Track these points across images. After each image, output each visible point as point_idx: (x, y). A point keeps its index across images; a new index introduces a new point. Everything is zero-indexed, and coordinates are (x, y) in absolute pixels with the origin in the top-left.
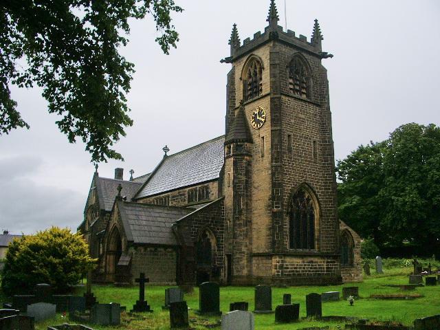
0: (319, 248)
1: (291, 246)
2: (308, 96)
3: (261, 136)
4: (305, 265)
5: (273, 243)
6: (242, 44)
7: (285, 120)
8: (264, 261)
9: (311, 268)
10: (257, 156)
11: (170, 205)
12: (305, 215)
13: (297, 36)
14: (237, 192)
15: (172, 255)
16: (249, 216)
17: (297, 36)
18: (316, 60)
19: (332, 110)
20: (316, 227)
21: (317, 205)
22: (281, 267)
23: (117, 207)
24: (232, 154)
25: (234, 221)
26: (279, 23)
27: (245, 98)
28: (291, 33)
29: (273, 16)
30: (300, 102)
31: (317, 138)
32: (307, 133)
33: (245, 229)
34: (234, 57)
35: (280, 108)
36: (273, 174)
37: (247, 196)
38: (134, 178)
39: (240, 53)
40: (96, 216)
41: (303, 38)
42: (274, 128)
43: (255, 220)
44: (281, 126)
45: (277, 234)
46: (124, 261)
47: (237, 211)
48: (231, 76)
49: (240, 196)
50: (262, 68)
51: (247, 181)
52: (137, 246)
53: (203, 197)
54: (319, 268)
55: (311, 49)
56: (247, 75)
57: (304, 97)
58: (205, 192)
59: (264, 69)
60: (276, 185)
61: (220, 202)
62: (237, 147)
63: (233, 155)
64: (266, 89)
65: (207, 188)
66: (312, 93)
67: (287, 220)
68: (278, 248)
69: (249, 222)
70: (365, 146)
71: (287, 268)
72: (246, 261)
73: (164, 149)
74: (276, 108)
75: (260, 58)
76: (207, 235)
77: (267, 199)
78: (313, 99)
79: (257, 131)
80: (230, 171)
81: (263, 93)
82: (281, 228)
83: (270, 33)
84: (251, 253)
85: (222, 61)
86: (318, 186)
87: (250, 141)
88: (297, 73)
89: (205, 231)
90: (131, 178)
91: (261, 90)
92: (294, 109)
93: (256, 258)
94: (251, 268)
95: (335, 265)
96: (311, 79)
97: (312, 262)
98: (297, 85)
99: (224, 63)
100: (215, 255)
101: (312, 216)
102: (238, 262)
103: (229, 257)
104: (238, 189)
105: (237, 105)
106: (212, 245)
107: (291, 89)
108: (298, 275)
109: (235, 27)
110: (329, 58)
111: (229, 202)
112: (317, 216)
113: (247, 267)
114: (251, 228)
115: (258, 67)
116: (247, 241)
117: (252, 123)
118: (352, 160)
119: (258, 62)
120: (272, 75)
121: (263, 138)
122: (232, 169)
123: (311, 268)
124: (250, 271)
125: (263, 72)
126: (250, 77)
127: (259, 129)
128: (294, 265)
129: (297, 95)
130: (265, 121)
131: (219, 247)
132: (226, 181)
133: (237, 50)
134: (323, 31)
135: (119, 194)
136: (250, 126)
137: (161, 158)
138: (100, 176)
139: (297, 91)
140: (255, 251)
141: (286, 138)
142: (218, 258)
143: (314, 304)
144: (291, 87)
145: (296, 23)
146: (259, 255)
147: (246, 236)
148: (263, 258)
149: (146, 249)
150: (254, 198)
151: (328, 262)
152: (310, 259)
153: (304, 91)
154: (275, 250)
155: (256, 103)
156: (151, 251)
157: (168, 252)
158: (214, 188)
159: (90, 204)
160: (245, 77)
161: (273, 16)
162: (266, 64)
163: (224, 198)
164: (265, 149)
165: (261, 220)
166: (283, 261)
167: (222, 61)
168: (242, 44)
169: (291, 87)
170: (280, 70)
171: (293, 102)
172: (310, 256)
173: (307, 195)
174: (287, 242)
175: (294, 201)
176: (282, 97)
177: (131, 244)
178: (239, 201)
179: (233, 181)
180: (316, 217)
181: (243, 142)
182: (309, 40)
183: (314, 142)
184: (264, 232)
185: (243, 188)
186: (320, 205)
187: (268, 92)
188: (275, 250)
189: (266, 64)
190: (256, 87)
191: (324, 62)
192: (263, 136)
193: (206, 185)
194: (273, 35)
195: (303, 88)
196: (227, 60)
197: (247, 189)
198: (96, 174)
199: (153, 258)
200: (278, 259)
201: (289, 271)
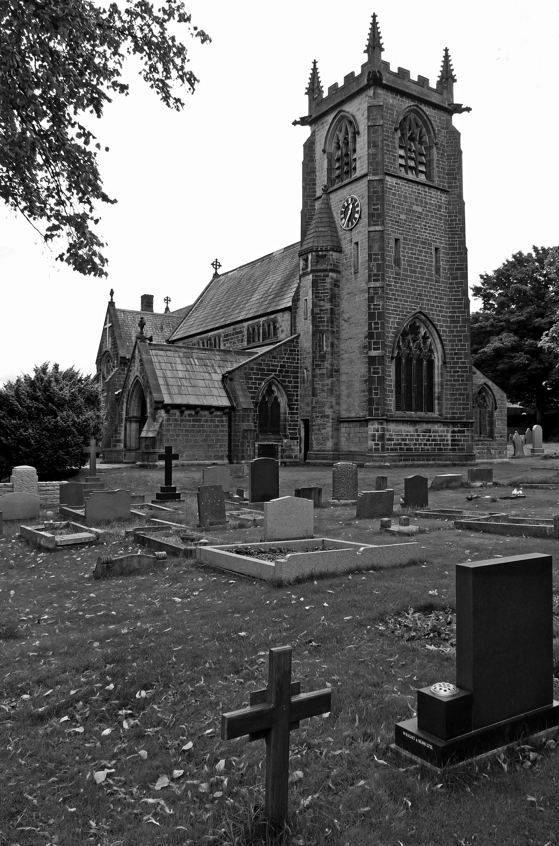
0: (440, 410)
1: (398, 408)
2: (428, 175)
3: (354, 241)
4: (418, 435)
5: (370, 401)
6: (325, 94)
7: (391, 213)
8: (357, 429)
9: (428, 440)
10: (348, 273)
11: (222, 347)
12: (420, 362)
13: (414, 77)
14: (316, 326)
15: (222, 421)
16: (335, 362)
17: (414, 77)
18: (444, 116)
19: (465, 198)
20: (437, 379)
21: (439, 346)
22: (382, 437)
23: (139, 352)
24: (309, 269)
25: (313, 370)
26: (384, 57)
27: (331, 181)
28: (403, 73)
29: (374, 45)
30: (415, 187)
31: (442, 244)
32: (425, 235)
33: (329, 381)
34: (314, 116)
35: (383, 196)
36: (371, 300)
37: (333, 332)
38: (172, 310)
39: (324, 108)
40: (114, 367)
41: (423, 81)
42: (372, 228)
43: (344, 368)
44: (383, 224)
45: (376, 389)
46: (148, 432)
47: (318, 357)
48: (309, 147)
49: (322, 332)
50: (356, 133)
51: (332, 310)
52: (168, 408)
53: (269, 335)
54: (441, 440)
55: (435, 99)
56: (334, 145)
57: (422, 178)
58: (272, 327)
59: (358, 133)
60: (375, 316)
61: (294, 343)
62: (319, 258)
63: (312, 271)
64: (362, 167)
65: (275, 322)
66: (435, 171)
67: (392, 369)
68: (377, 409)
69: (335, 372)
70: (525, 254)
71: (392, 440)
72: (330, 429)
73: (213, 264)
74: (377, 196)
75: (354, 117)
76: (273, 392)
77: (362, 336)
78: (436, 183)
79: (348, 234)
80: (307, 295)
81: (358, 174)
82: (382, 380)
83: (369, 73)
84: (339, 418)
85: (295, 123)
86: (441, 319)
87: (339, 250)
88: (412, 139)
89: (270, 386)
90: (167, 309)
91: (355, 168)
92: (405, 197)
93: (346, 425)
94: (338, 438)
95: (465, 436)
96: (434, 149)
97: (429, 431)
98: (412, 159)
99: (298, 126)
100: (285, 420)
101: (431, 363)
102: (319, 430)
103: (306, 422)
104: (320, 322)
105: (319, 192)
106: (282, 405)
107: (401, 165)
108: (408, 449)
109: (315, 66)
110: (465, 113)
111: (306, 343)
112: (438, 363)
113: (332, 438)
114: (338, 381)
115: (350, 130)
116: (334, 400)
117: (342, 223)
118: (502, 278)
119: (351, 123)
120: (372, 144)
121: (357, 243)
122: (310, 292)
123: (428, 440)
124: (337, 444)
125: (358, 139)
126: (338, 147)
127: (351, 230)
128: (402, 435)
129: (411, 176)
130: (360, 217)
131: (290, 409)
132: (301, 312)
133: (318, 105)
134: (457, 70)
135: (142, 333)
136: (338, 226)
137: (211, 278)
138: (117, 306)
139: (412, 168)
140: (344, 414)
141: (392, 244)
142: (290, 425)
143: (416, 493)
144: (402, 162)
145: (412, 57)
146: (349, 421)
147: (331, 391)
148: (355, 424)
149: (182, 412)
150: (344, 335)
151: (453, 432)
152: (426, 426)
153: (422, 168)
154: (374, 412)
155: (347, 189)
156: (190, 415)
157: (216, 416)
158: (284, 320)
159: (104, 350)
160: (332, 148)
161: (374, 45)
162: (363, 125)
163: (299, 336)
164: (360, 260)
165: (353, 367)
166: (383, 429)
167: (295, 123)
168: (325, 94)
169: (402, 162)
170: (386, 133)
171: (404, 187)
172: (428, 422)
173: (423, 331)
174: (391, 400)
175: (403, 341)
176: (388, 178)
177: (160, 405)
178: (321, 340)
179: (313, 310)
180: (436, 363)
181: (327, 250)
182: (433, 84)
183: (437, 249)
184: (359, 386)
185: (326, 322)
186: (443, 346)
187: (365, 171)
188: (374, 412)
189: (363, 125)
190: (347, 164)
191: (457, 120)
192: (356, 241)
193: (273, 316)
194: (376, 76)
195: (421, 163)
196: (303, 121)
197: (332, 322)
198: (111, 304)
199: (194, 426)
200: (376, 426)
201: (394, 444)
